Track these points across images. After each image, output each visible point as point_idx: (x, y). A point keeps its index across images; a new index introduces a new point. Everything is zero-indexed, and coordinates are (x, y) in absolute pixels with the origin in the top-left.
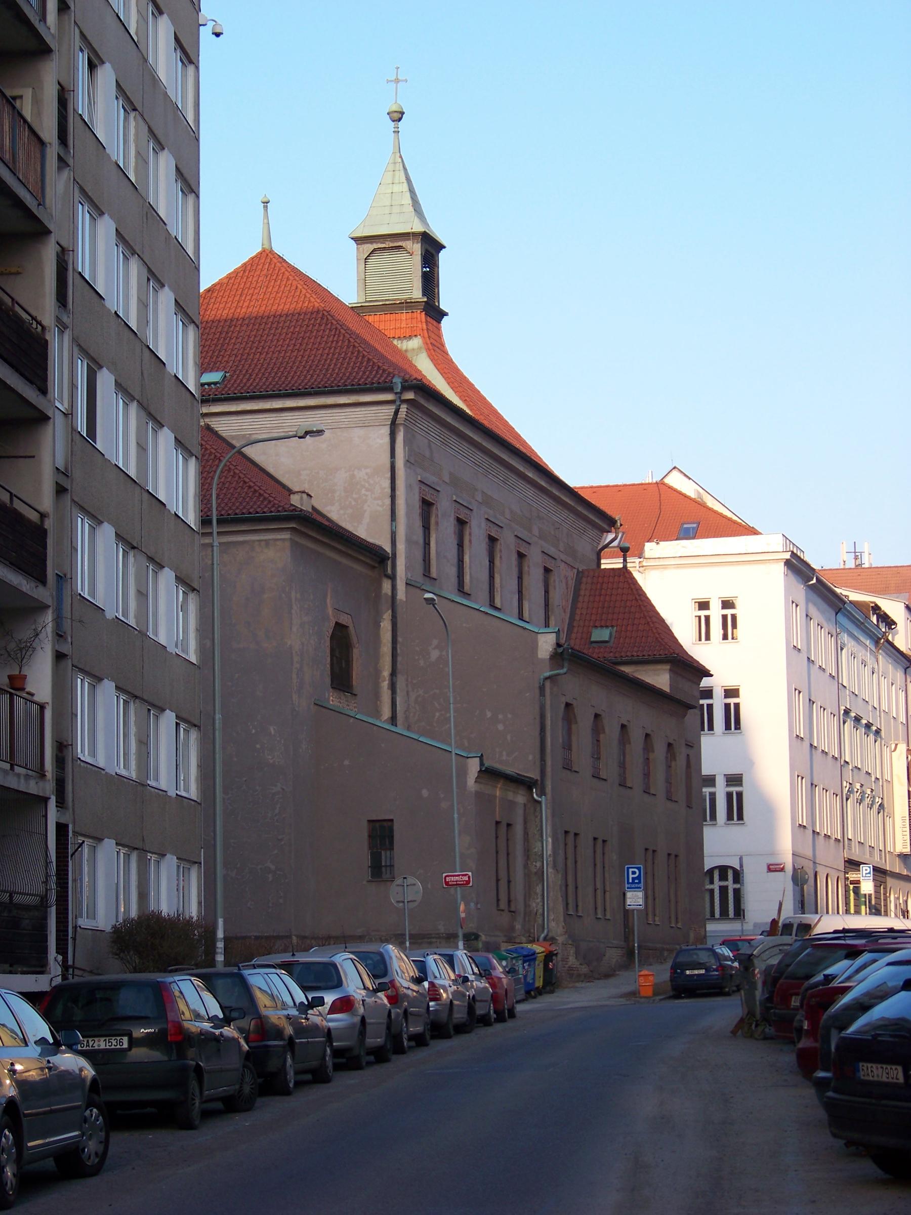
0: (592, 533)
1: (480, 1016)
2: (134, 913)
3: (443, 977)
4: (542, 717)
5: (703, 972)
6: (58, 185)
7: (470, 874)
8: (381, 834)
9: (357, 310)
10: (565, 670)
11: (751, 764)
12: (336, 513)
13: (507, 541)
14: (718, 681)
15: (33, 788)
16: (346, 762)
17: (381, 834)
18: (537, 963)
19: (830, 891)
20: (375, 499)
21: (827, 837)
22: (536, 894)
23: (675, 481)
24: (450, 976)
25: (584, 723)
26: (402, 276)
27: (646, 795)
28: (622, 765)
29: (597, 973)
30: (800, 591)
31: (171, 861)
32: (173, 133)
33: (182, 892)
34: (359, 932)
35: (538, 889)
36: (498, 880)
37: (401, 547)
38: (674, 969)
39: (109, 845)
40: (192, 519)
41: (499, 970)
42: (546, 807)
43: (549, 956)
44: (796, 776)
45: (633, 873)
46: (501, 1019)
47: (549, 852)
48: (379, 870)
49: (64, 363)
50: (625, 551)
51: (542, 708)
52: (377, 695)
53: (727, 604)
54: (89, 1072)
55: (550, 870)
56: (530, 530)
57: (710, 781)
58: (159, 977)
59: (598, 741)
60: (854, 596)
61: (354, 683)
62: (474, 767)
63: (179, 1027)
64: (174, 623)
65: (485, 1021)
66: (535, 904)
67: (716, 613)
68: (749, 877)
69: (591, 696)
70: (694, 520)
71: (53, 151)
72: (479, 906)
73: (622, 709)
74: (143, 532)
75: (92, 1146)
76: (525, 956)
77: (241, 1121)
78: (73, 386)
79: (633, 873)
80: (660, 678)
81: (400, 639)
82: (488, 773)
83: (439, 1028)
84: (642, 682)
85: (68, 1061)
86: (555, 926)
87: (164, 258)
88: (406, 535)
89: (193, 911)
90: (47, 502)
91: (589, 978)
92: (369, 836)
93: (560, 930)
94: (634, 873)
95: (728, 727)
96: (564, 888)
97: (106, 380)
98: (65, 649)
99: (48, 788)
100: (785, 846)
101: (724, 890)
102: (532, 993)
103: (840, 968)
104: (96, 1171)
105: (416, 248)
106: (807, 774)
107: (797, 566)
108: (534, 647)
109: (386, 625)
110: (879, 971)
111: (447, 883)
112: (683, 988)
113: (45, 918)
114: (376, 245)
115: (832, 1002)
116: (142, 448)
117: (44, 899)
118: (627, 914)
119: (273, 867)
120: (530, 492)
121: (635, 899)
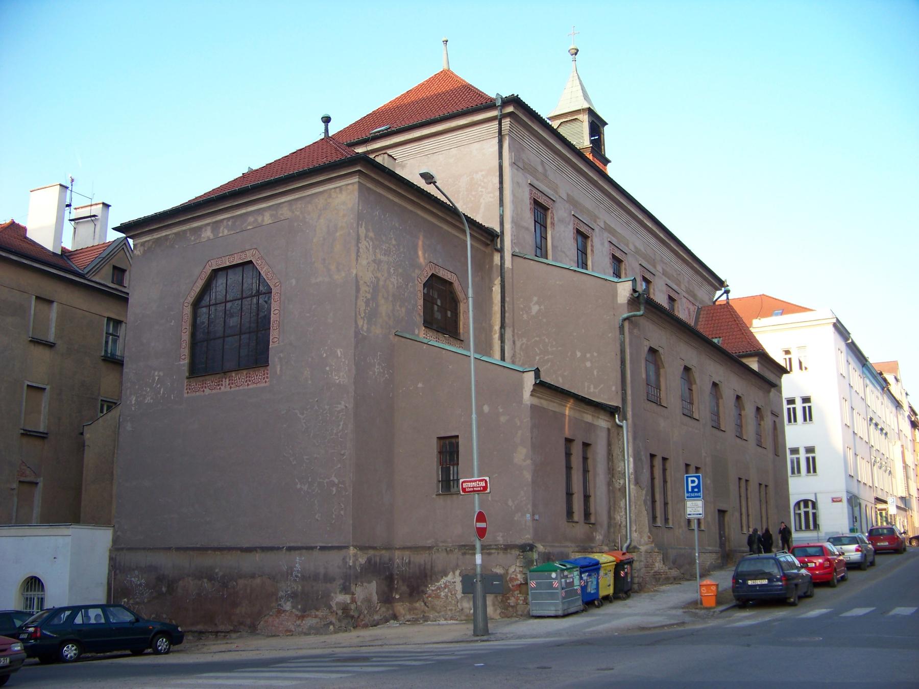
0: (709, 288)
4: (623, 352)
5: (765, 582)
7: (487, 478)
10: (641, 312)
16: (420, 385)
18: (602, 572)
20: (489, 193)
21: (865, 484)
22: (621, 508)
27: (738, 440)
34: (429, 543)
35: (622, 504)
36: (569, 495)
37: (508, 226)
38: (735, 579)
42: (627, 432)
43: (619, 566)
47: (631, 470)
51: (622, 344)
55: (632, 487)
56: (655, 267)
59: (690, 390)
61: (461, 331)
62: (529, 380)
68: (820, 505)
72: (537, 517)
76: (582, 567)
81: (507, 299)
82: (541, 386)
88: (513, 217)
91: (676, 580)
92: (440, 453)
93: (645, 539)
94: (693, 482)
95: (805, 420)
96: (649, 503)
101: (806, 513)
102: (596, 602)
106: (852, 447)
108: (615, 295)
109: (497, 289)
111: (464, 490)
119: (336, 481)
120: (653, 240)
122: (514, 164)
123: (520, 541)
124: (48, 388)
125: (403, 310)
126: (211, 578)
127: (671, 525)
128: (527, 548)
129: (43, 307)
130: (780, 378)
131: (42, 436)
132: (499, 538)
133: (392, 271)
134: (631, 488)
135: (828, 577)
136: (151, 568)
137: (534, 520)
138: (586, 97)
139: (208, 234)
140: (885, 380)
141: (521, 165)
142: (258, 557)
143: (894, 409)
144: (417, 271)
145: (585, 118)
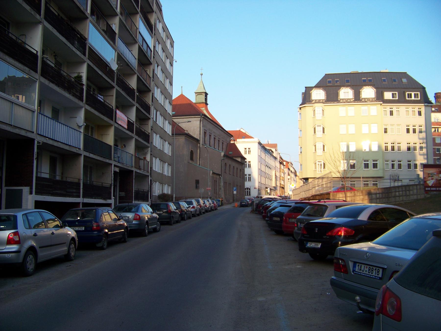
1: (212, 209)
2: (161, 193)
3: (207, 204)
6: (152, 83)
8: (197, 182)
9: (195, 103)
11: (252, 173)
12: (191, 134)
13: (217, 138)
14: (247, 160)
15: (147, 174)
17: (197, 182)
19: (263, 192)
23: (242, 130)
24: (208, 203)
25: (228, 166)
26: (202, 98)
28: (233, 172)
29: (229, 203)
30: (260, 147)
31: (166, 185)
32: (169, 76)
33: (168, 190)
37: (201, 139)
39: (158, 183)
40: (170, 134)
41: (215, 203)
43: (222, 201)
44: (259, 174)
45: (235, 188)
46: (215, 210)
48: (197, 187)
49: (153, 111)
50: (234, 140)
52: (197, 161)
53: (249, 149)
54: (158, 217)
57: (246, 175)
58: (167, 203)
60: (268, 148)
62: (211, 172)
63: (170, 210)
64: (167, 149)
65: (213, 210)
66: (220, 193)
67: (247, 150)
69: (229, 162)
70: (244, 136)
71: (152, 79)
73: (234, 164)
74: (163, 136)
75: (158, 228)
77: (179, 225)
78: (154, 114)
79: (235, 188)
80: (239, 160)
83: (207, 211)
84: (236, 160)
85: (155, 215)
86: (223, 196)
87: (167, 95)
89: (170, 193)
90: (150, 131)
91: (228, 204)
97: (158, 113)
98: (152, 153)
99: (149, 174)
100: (257, 185)
103: (268, 203)
104: (158, 231)
105: (204, 94)
107: (260, 143)
108: (221, 154)
109: (199, 151)
110: (275, 204)
112: (242, 206)
113: (148, 194)
114: (198, 94)
115: (268, 208)
116: (163, 123)
117: (148, 191)
118: (233, 194)
120: (220, 131)
121: (235, 192)
122: (202, 126)
134: (222, 188)
143: (274, 160)
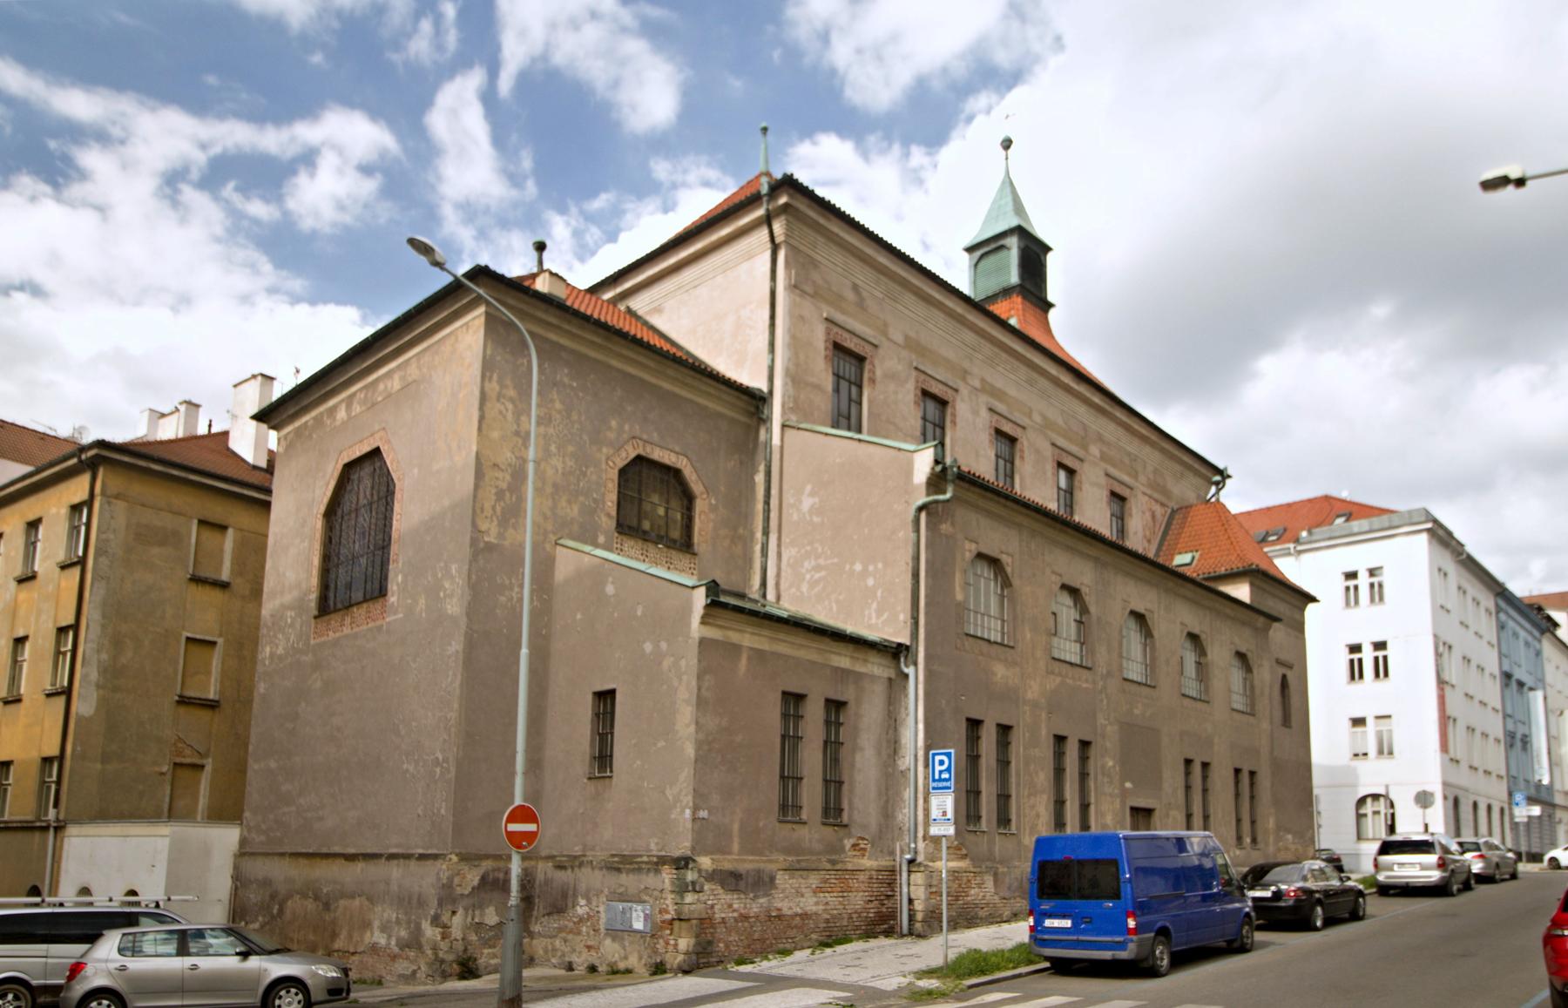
4: (917, 558)
10: (948, 495)
62: (700, 598)
72: (703, 814)
94: (942, 763)
95: (1377, 675)
108: (908, 471)
109: (760, 478)
114: (985, 249)
122: (794, 287)
123: (677, 853)
124: (220, 641)
125: (576, 508)
126: (316, 898)
127: (1014, 830)
128: (682, 863)
129: (209, 536)
130: (1303, 610)
131: (212, 705)
132: (653, 846)
133: (553, 448)
135: (1343, 907)
136: (266, 882)
137: (694, 820)
138: (1019, 208)
139: (342, 414)
140: (1549, 619)
141: (809, 289)
142: (359, 866)
144: (605, 450)
145: (1013, 242)
